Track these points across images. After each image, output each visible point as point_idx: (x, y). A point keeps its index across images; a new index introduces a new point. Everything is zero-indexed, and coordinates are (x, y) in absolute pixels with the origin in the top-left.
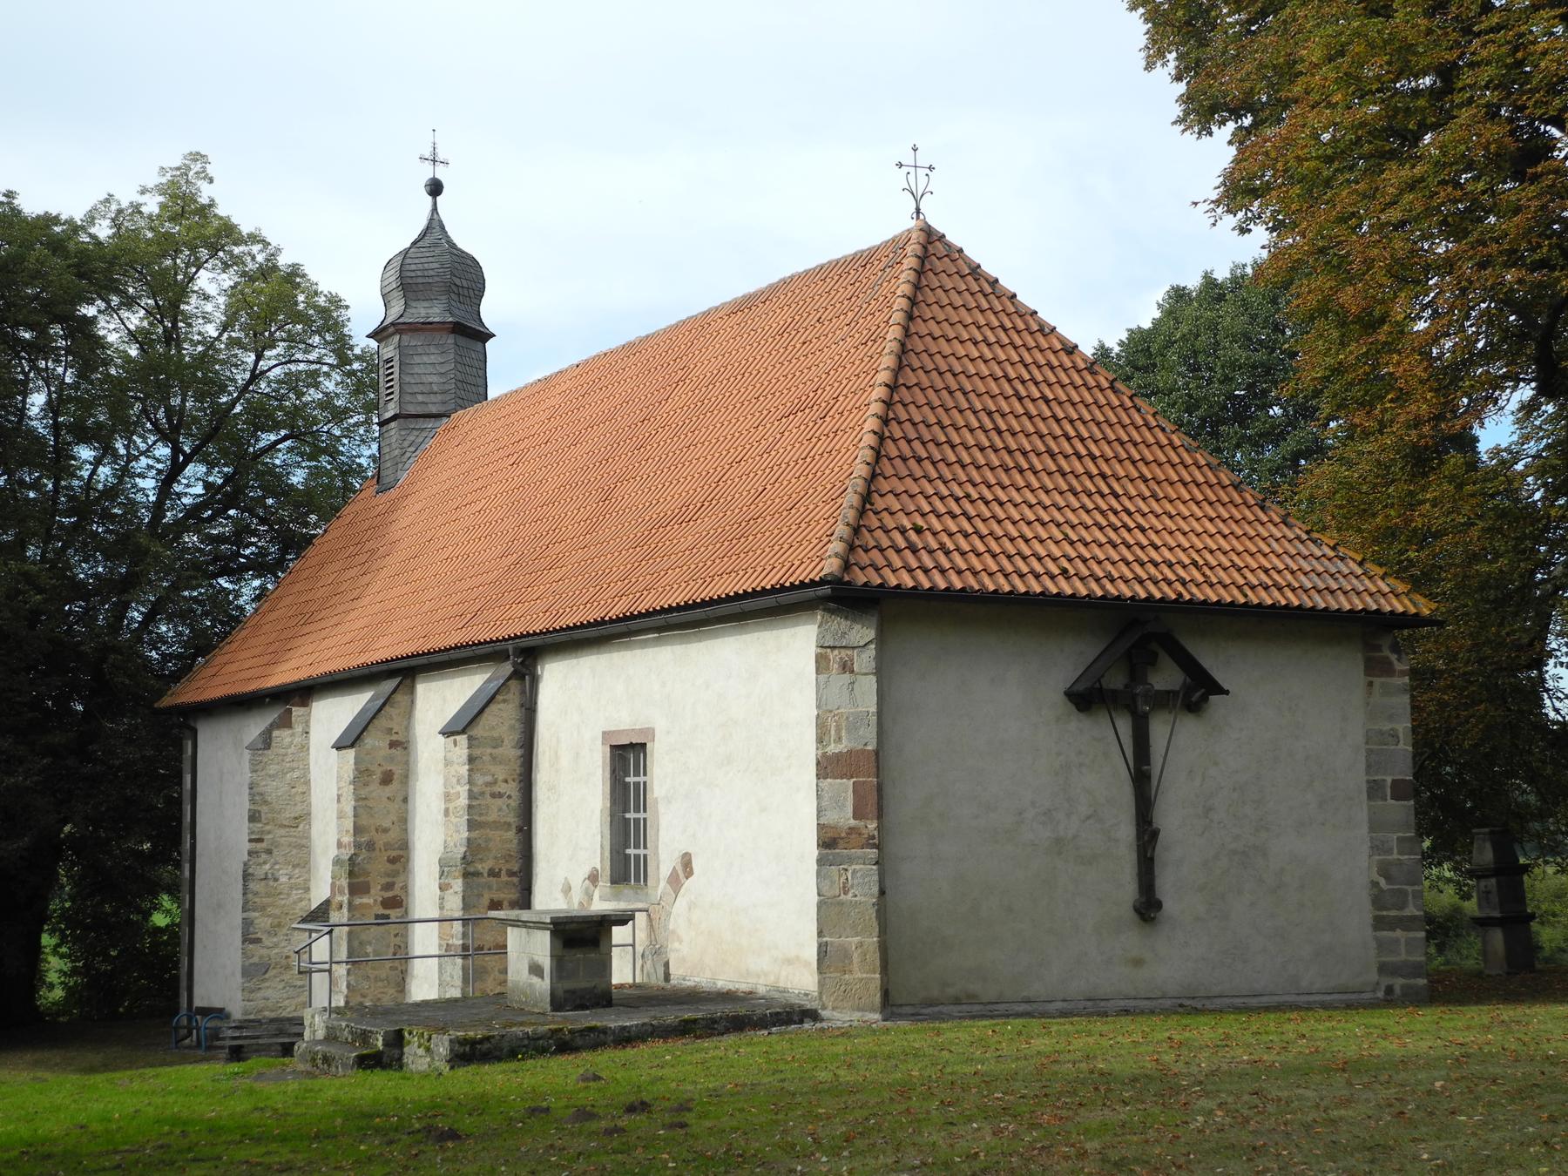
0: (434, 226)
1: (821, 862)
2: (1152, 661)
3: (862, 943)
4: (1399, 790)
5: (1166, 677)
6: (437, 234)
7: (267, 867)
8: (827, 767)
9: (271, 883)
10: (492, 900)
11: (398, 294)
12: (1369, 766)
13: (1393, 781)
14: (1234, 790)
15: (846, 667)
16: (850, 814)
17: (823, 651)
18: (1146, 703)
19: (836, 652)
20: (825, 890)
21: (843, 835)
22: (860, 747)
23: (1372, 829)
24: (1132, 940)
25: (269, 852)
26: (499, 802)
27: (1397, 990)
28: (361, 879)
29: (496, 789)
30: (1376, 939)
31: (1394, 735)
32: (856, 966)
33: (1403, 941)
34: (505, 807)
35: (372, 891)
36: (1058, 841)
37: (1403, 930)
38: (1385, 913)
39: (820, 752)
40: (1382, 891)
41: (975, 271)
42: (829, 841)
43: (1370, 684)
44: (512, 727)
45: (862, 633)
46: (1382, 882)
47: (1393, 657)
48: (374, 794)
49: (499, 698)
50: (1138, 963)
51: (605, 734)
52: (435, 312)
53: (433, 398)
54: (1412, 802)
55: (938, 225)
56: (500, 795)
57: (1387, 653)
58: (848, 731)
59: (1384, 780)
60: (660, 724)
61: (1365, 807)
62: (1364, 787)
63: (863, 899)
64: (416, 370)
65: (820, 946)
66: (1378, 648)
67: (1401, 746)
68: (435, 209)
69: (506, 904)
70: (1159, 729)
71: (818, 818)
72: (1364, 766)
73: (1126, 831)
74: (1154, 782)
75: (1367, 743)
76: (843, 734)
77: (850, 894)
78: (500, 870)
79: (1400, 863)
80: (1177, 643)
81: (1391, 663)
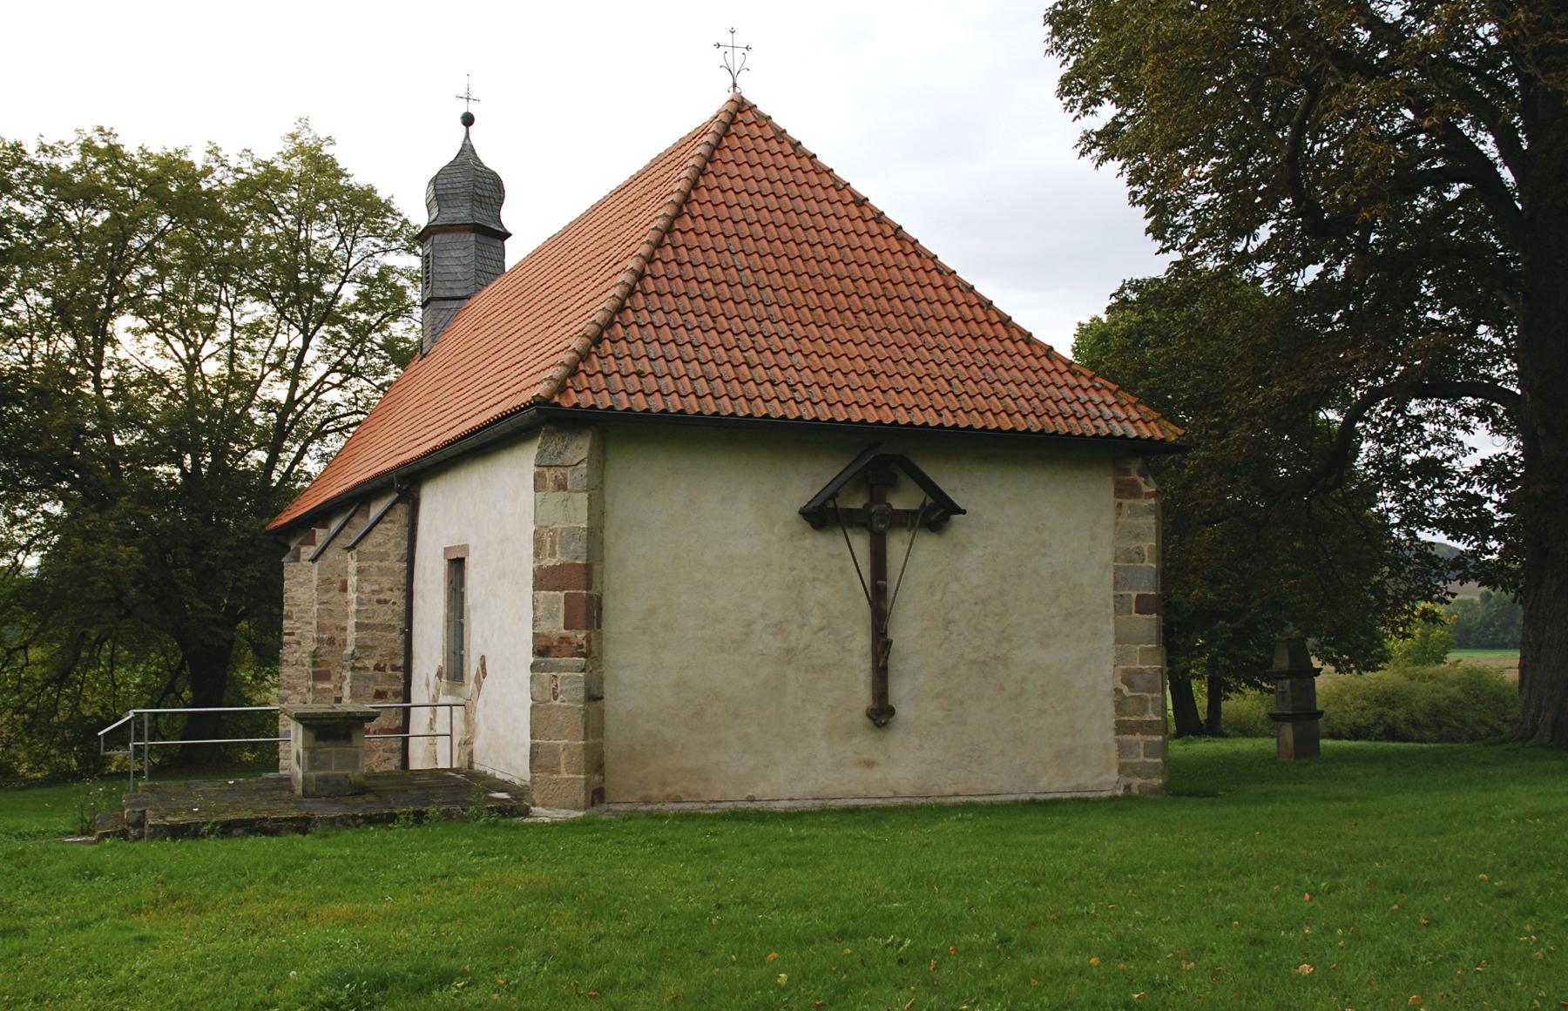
0: (467, 150)
1: (534, 667)
2: (892, 484)
3: (569, 743)
4: (1143, 605)
5: (905, 499)
6: (468, 153)
7: (297, 655)
8: (544, 579)
9: (300, 668)
10: (377, 691)
11: (434, 203)
12: (1116, 583)
13: (1138, 595)
14: (976, 604)
15: (561, 486)
16: (562, 625)
17: (540, 469)
18: (882, 522)
19: (552, 471)
20: (536, 696)
21: (555, 644)
22: (571, 561)
23: (1118, 641)
24: (865, 743)
25: (298, 643)
26: (385, 607)
27: (1135, 791)
28: (323, 668)
29: (382, 597)
30: (1118, 741)
31: (1140, 553)
32: (563, 768)
33: (1142, 744)
34: (390, 612)
35: (332, 678)
36: (789, 651)
37: (1143, 734)
38: (1126, 718)
39: (536, 564)
40: (1125, 698)
41: (780, 135)
42: (543, 649)
43: (1120, 505)
44: (397, 545)
45: (579, 450)
46: (1125, 689)
47: (1141, 480)
48: (334, 600)
49: (387, 518)
50: (870, 764)
51: (447, 550)
52: (462, 214)
53: (458, 285)
54: (1154, 616)
55: (751, 97)
56: (386, 602)
57: (1135, 476)
58: (562, 546)
59: (1130, 595)
60: (473, 542)
61: (1111, 620)
62: (1111, 601)
63: (570, 704)
64: (446, 263)
65: (533, 746)
66: (1127, 472)
67: (1146, 563)
68: (468, 133)
69: (390, 693)
70: (896, 545)
71: (534, 626)
72: (1112, 582)
73: (862, 641)
74: (890, 595)
75: (1115, 561)
76: (557, 548)
77: (559, 700)
78: (385, 665)
79: (1142, 672)
80: (918, 470)
81: (1139, 487)
